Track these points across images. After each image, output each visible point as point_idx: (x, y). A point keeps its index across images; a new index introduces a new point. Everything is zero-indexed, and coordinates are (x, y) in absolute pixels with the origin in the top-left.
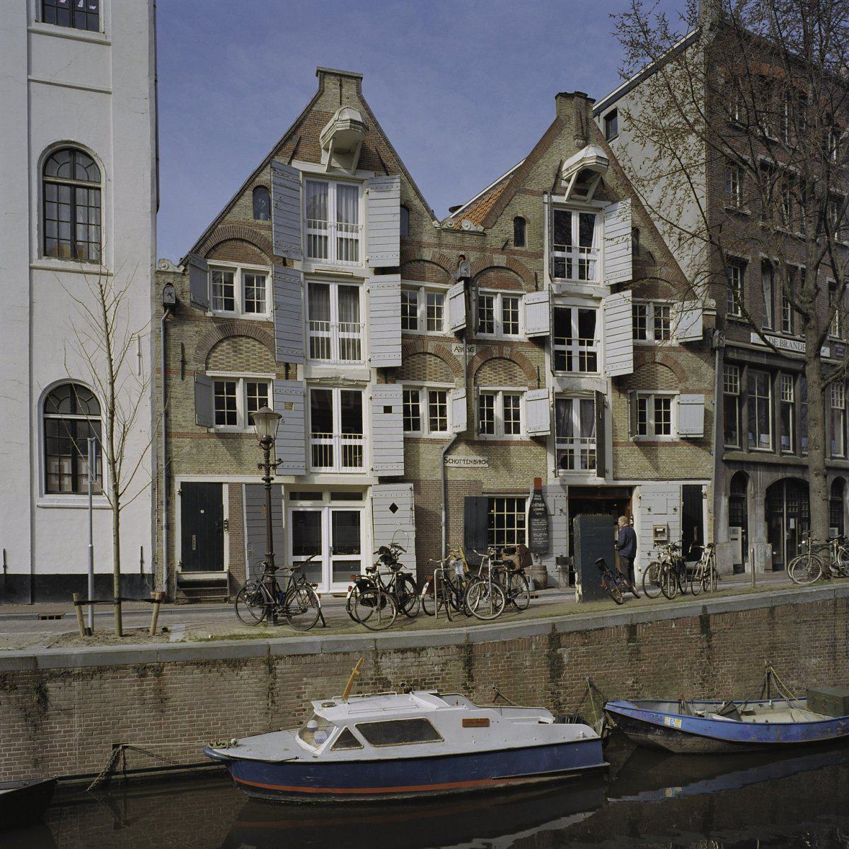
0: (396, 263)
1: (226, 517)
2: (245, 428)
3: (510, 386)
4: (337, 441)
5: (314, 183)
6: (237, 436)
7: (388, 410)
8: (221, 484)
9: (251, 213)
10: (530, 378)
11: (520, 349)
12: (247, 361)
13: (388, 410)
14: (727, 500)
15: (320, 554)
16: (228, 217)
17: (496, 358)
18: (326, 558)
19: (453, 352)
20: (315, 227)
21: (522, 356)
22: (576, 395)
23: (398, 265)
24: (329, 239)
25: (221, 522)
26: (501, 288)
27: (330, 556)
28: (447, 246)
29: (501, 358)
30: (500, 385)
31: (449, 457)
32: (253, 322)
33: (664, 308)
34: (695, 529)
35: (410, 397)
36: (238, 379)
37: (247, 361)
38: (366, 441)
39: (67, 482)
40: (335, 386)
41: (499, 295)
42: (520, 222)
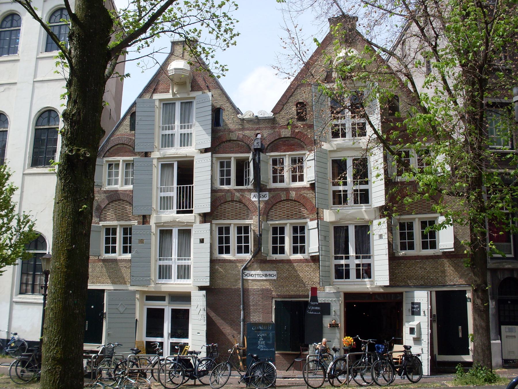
0: (209, 146)
1: (105, 311)
2: (420, 251)
3: (295, 219)
4: (353, 261)
5: (166, 104)
6: (115, 261)
7: (141, 241)
8: (103, 291)
9: (128, 128)
10: (311, 212)
11: (302, 192)
12: (123, 214)
13: (141, 241)
14: (494, 303)
15: (188, 338)
16: (118, 133)
17: (284, 200)
18: (167, 340)
19: (252, 199)
20: (166, 129)
21: (304, 197)
22: (350, 222)
23: (210, 146)
24: (193, 135)
25: (103, 314)
26: (288, 151)
27: (168, 339)
28: (248, 129)
29: (288, 200)
30: (288, 219)
31: (247, 272)
32: (126, 191)
33: (116, 164)
34: (460, 327)
35: (224, 231)
36: (286, 224)
37: (123, 214)
38: (191, 262)
39: (30, 287)
40: (173, 226)
41: (287, 156)
42: (301, 105)
